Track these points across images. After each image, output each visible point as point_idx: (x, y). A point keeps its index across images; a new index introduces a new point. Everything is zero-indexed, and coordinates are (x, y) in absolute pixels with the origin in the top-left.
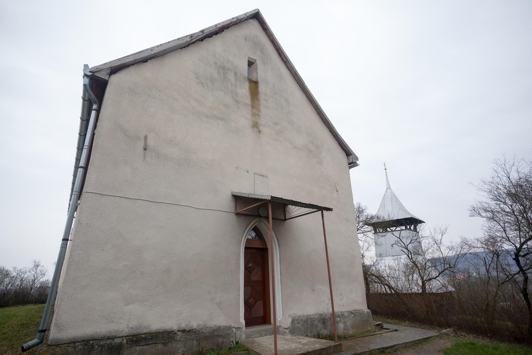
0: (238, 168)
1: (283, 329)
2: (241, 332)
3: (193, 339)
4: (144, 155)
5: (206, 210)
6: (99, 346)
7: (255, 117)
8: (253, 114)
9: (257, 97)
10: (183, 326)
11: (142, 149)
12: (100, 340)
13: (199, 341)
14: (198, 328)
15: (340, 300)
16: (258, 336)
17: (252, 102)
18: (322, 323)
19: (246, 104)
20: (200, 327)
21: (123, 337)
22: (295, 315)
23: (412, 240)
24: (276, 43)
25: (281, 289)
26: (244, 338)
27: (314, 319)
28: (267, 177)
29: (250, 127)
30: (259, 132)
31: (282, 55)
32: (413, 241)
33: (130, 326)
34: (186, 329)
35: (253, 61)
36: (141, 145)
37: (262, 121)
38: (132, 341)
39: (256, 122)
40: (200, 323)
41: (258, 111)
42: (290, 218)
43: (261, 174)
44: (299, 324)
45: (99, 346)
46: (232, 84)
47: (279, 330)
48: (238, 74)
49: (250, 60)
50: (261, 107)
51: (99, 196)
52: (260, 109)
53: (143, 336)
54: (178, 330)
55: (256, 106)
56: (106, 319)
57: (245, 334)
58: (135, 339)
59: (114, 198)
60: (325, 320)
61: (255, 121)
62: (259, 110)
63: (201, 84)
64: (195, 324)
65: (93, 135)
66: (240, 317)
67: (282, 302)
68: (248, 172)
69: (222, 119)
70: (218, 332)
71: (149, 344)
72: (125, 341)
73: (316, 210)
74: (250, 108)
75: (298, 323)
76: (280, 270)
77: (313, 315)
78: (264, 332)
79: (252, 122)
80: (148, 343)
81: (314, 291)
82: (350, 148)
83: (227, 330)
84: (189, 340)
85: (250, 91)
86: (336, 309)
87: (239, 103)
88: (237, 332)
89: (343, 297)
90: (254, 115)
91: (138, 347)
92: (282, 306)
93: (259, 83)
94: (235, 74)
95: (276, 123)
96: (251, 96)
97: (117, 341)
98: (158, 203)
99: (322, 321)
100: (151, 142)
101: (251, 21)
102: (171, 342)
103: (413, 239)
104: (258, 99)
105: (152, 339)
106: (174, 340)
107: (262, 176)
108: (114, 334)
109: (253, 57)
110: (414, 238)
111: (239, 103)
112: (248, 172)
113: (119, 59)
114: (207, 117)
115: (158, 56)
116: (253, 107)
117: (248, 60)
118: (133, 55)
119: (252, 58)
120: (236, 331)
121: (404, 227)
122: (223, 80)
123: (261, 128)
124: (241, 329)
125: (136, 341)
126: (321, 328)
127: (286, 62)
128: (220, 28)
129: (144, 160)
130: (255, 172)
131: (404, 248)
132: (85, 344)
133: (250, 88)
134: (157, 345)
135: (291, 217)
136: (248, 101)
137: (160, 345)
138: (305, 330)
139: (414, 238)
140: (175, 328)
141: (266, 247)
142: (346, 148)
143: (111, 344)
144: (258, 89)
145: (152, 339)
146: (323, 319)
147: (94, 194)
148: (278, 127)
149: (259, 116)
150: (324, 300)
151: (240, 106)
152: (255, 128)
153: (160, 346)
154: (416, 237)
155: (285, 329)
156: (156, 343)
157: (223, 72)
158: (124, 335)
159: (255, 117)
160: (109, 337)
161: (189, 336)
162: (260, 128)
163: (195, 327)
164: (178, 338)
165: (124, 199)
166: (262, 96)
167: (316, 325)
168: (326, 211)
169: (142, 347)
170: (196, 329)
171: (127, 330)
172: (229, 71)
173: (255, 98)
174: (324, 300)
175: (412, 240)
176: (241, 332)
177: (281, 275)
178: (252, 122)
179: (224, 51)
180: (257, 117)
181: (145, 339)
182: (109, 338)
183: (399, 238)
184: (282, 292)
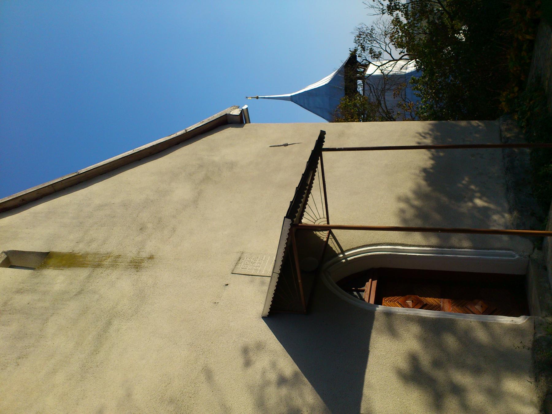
7: (119, 264)
8: (113, 266)
19: (89, 276)
23: (386, 51)
29: (139, 273)
30: (151, 258)
32: (389, 50)
37: (131, 252)
39: (131, 262)
41: (109, 257)
42: (326, 220)
43: (235, 262)
46: (39, 300)
48: (21, 287)
50: (103, 250)
52: (106, 253)
55: (97, 260)
61: (127, 264)
62: (108, 255)
63: (20, 360)
65: (410, 246)
68: (227, 285)
69: (109, 323)
73: (319, 161)
74: (99, 270)
79: (129, 268)
87: (82, 290)
90: (114, 265)
93: (51, 250)
94: (19, 291)
95: (141, 229)
103: (385, 50)
104: (85, 256)
110: (384, 47)
111: (82, 290)
112: (227, 285)
114: (96, 351)
116: (98, 265)
121: (358, 81)
122: (25, 315)
127: (23, 200)
130: (230, 272)
131: (396, 63)
135: (325, 216)
136: (82, 273)
139: (384, 47)
144: (63, 253)
148: (150, 225)
149: (119, 256)
151: (90, 288)
152: (143, 264)
154: (381, 43)
157: (9, 315)
159: (119, 264)
162: (144, 256)
166: (80, 248)
168: (324, 143)
172: (9, 303)
173: (81, 260)
175: (386, 51)
178: (129, 270)
180: (120, 260)
183: (379, 67)
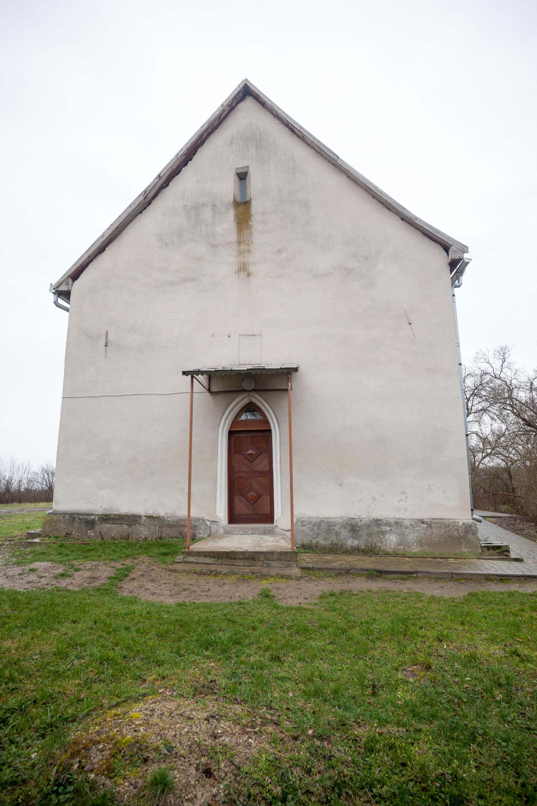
0: (214, 336)
1: (281, 531)
2: (218, 526)
3: (156, 525)
4: (106, 352)
5: (173, 395)
6: (79, 519)
9: (248, 224)
10: (150, 513)
11: (104, 347)
12: (80, 514)
13: (161, 527)
14: (166, 517)
15: (400, 500)
16: (241, 533)
17: (238, 236)
18: (349, 530)
20: (168, 515)
21: (96, 515)
22: (302, 516)
24: (281, 116)
25: (281, 481)
26: (223, 533)
27: (334, 524)
28: (260, 335)
31: (295, 130)
33: (103, 507)
34: (153, 515)
35: (244, 171)
36: (103, 342)
38: (103, 519)
40: (168, 511)
44: (304, 527)
45: (79, 519)
47: (274, 531)
49: (240, 171)
51: (72, 399)
53: (112, 516)
54: (145, 515)
56: (85, 500)
57: (224, 529)
58: (105, 518)
59: (83, 398)
60: (357, 526)
64: (162, 512)
66: (217, 510)
67: (281, 497)
69: (191, 280)
70: (183, 522)
71: (116, 523)
72: (97, 518)
74: (235, 246)
75: (303, 526)
76: (280, 457)
77: (336, 518)
78: (250, 530)
80: (115, 522)
81: (341, 486)
82: (444, 235)
83: (195, 521)
84: (152, 526)
85: (236, 220)
86: (193, 515)
88: (213, 525)
89: (406, 497)
90: (240, 253)
91: (107, 525)
92: (282, 502)
95: (280, 251)
96: (238, 227)
97: (92, 517)
98: (122, 397)
99: (349, 527)
100: (111, 337)
101: (242, 105)
102: (135, 525)
104: (249, 227)
105: (118, 519)
106: (138, 523)
107: (252, 336)
108: (91, 512)
109: (241, 164)
113: (74, 265)
115: (115, 237)
117: (237, 173)
118: (86, 252)
119: (241, 168)
120: (211, 524)
123: (252, 269)
124: (218, 523)
125: (106, 519)
126: (347, 537)
127: (303, 137)
128: (185, 154)
129: (106, 356)
132: (71, 516)
133: (237, 216)
134: (123, 525)
136: (233, 237)
137: (125, 525)
138: (315, 536)
140: (143, 513)
141: (269, 428)
142: (440, 240)
143: (87, 519)
145: (118, 519)
146: (351, 525)
147: (69, 398)
150: (362, 499)
153: (125, 527)
155: (284, 532)
156: (121, 524)
158: (99, 513)
160: (88, 514)
161: (153, 522)
163: (162, 515)
164: (142, 522)
165: (91, 398)
167: (337, 532)
169: (110, 525)
170: (164, 516)
171: (101, 511)
174: (362, 499)
176: (218, 526)
177: (280, 463)
179: (198, 182)
181: (113, 519)
182: (88, 515)
184: (281, 485)
